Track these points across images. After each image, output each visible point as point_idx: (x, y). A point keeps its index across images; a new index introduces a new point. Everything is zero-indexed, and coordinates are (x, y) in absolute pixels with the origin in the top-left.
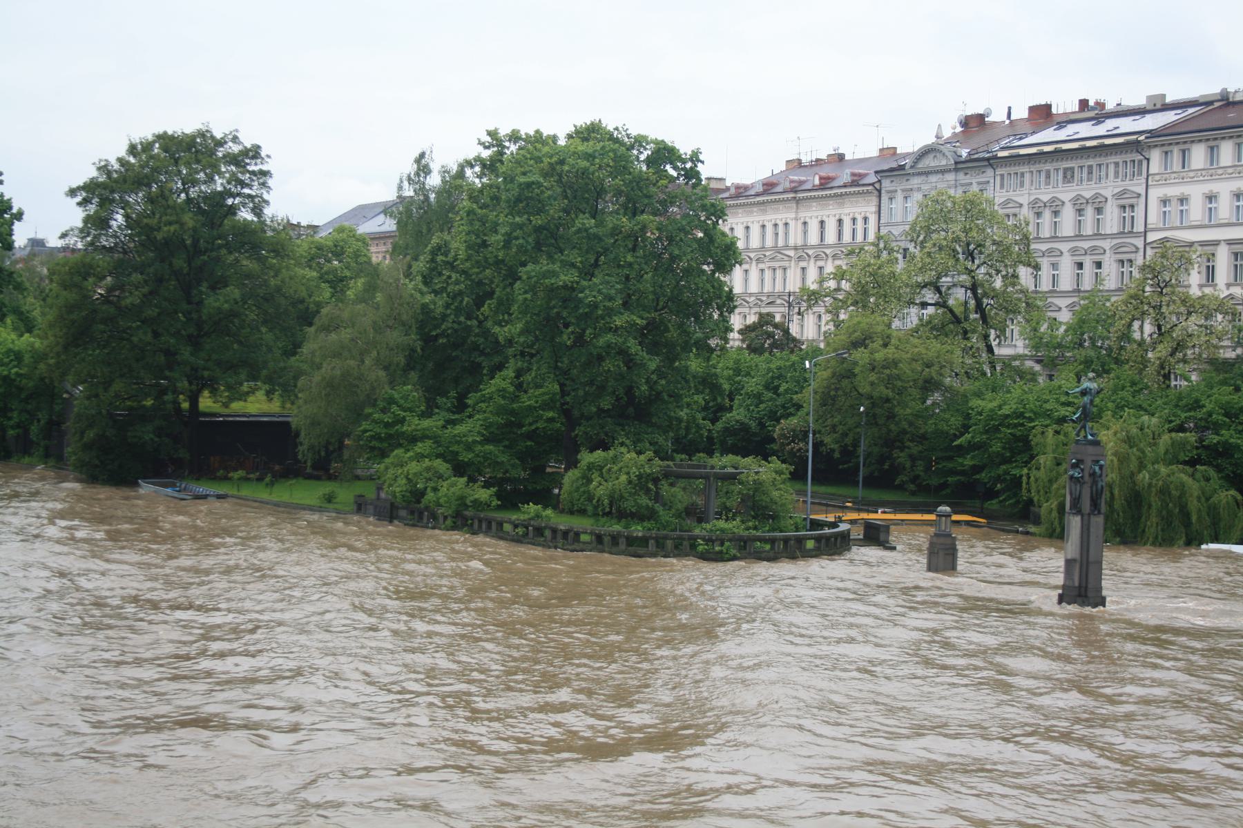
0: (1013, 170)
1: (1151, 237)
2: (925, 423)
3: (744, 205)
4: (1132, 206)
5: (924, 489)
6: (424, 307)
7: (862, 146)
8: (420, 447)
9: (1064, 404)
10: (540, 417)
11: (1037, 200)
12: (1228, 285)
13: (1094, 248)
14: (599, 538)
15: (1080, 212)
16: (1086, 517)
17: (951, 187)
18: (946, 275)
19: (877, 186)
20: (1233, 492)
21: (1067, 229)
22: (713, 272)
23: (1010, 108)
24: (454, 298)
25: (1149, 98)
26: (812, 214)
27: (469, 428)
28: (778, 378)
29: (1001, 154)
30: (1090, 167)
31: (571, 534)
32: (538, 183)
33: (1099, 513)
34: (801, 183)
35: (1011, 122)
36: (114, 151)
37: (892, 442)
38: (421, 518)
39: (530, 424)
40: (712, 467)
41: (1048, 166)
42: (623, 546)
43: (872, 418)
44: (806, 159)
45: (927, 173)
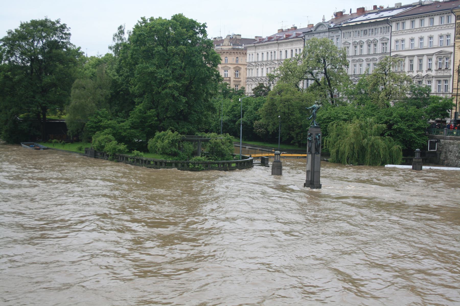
0: (347, 31)
1: (393, 54)
2: (301, 122)
6: (115, 80)
7: (302, 25)
8: (106, 131)
9: (346, 114)
10: (153, 120)
11: (355, 42)
12: (417, 71)
14: (156, 163)
15: (369, 46)
16: (313, 155)
17: (319, 37)
19: (304, 38)
23: (351, 9)
24: (126, 78)
25: (396, 4)
26: (283, 48)
27: (127, 124)
28: (258, 106)
29: (343, 25)
30: (372, 29)
31: (147, 162)
32: (144, 34)
34: (280, 37)
35: (351, 14)
36: (15, 26)
37: (291, 128)
38: (104, 156)
39: (150, 122)
40: (205, 137)
41: (359, 29)
42: (164, 166)
44: (284, 29)
45: (319, 33)
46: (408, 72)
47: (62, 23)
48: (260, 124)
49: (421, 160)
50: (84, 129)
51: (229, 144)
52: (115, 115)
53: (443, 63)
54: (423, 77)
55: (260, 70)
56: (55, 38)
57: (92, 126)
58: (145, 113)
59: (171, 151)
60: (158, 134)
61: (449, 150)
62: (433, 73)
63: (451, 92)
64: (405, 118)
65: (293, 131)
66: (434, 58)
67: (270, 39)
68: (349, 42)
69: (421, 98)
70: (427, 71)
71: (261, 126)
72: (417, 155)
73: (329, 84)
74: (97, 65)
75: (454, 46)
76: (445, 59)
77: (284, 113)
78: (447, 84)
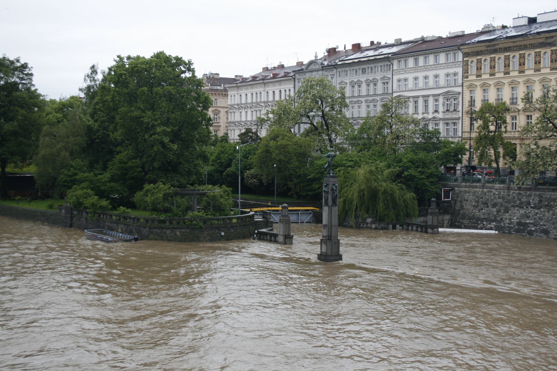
0: (343, 69)
1: (395, 95)
3: (245, 86)
4: (387, 83)
5: (299, 197)
7: (290, 62)
8: (83, 185)
9: (350, 161)
12: (423, 113)
13: (374, 100)
15: (368, 85)
17: (317, 76)
18: (312, 111)
20: (412, 194)
21: (364, 93)
22: (202, 110)
25: (396, 40)
27: (107, 176)
29: (339, 63)
30: (372, 68)
33: (336, 205)
34: (266, 76)
35: (346, 51)
39: (132, 174)
40: (199, 190)
41: (356, 68)
43: (279, 170)
44: (270, 67)
45: (312, 71)
46: (413, 114)
47: (22, 62)
48: (252, 175)
49: (437, 210)
50: (56, 183)
51: (226, 197)
52: (91, 167)
53: (451, 105)
54: (430, 120)
55: (249, 113)
56: (15, 79)
57: (67, 180)
58: (126, 163)
59: (163, 206)
60: (147, 187)
61: (464, 199)
62: (440, 115)
63: (460, 135)
64: (415, 164)
65: (291, 181)
66: (441, 99)
67: (254, 78)
68: (346, 81)
69: (430, 141)
70: (433, 113)
71: (254, 176)
72: (433, 205)
73: (328, 129)
74: (60, 110)
75: (462, 86)
76: (453, 100)
77: (280, 161)
78: (455, 127)
